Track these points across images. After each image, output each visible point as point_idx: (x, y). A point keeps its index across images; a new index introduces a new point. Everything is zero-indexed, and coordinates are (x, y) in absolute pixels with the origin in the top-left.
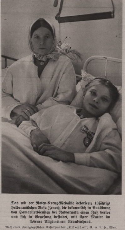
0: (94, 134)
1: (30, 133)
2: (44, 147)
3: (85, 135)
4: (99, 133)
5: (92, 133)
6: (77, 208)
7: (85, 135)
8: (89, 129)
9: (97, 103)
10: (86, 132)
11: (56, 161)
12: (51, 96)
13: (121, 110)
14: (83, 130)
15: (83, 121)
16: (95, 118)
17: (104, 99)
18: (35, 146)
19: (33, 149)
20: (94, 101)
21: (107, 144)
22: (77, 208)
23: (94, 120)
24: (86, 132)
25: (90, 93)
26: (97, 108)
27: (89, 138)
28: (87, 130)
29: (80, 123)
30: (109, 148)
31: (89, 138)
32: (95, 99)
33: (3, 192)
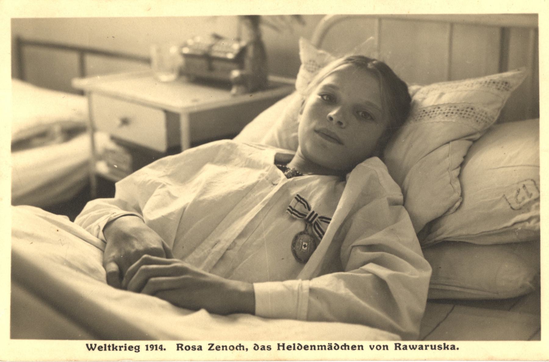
0: (327, 220)
1: (103, 231)
2: (143, 267)
3: (298, 226)
4: (344, 215)
5: (321, 218)
6: (317, 348)
7: (298, 226)
8: (313, 205)
9: (340, 123)
10: (302, 215)
11: (186, 311)
12: (172, 71)
13: (374, 233)
14: (292, 210)
15: (296, 184)
16: (335, 177)
17: (362, 113)
18: (113, 267)
19: (105, 281)
20: (331, 119)
21: (370, 247)
22: (317, 348)
23: (334, 182)
24: (302, 215)
25: (320, 97)
26: (339, 142)
27: (312, 236)
28: (304, 210)
29: (284, 190)
30: (376, 261)
31: (312, 236)
32: (333, 113)
33: (539, 339)
